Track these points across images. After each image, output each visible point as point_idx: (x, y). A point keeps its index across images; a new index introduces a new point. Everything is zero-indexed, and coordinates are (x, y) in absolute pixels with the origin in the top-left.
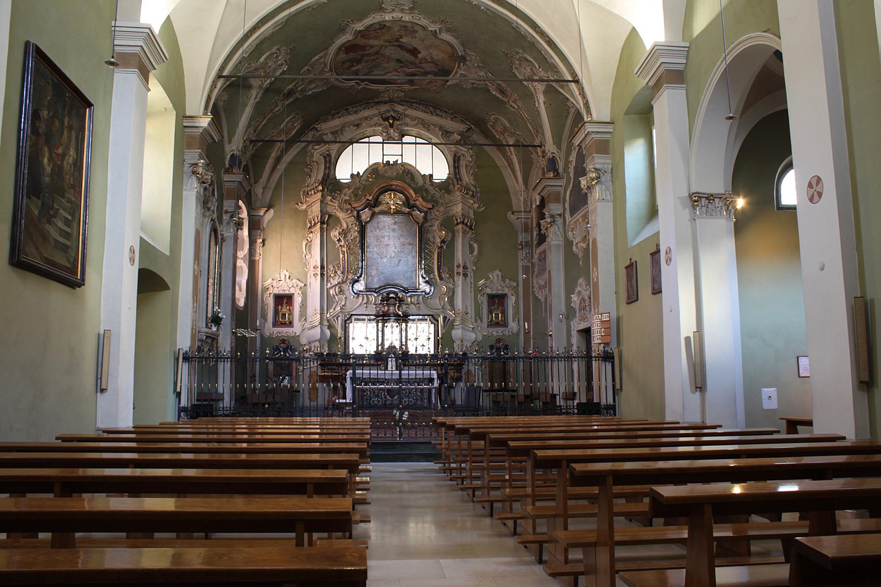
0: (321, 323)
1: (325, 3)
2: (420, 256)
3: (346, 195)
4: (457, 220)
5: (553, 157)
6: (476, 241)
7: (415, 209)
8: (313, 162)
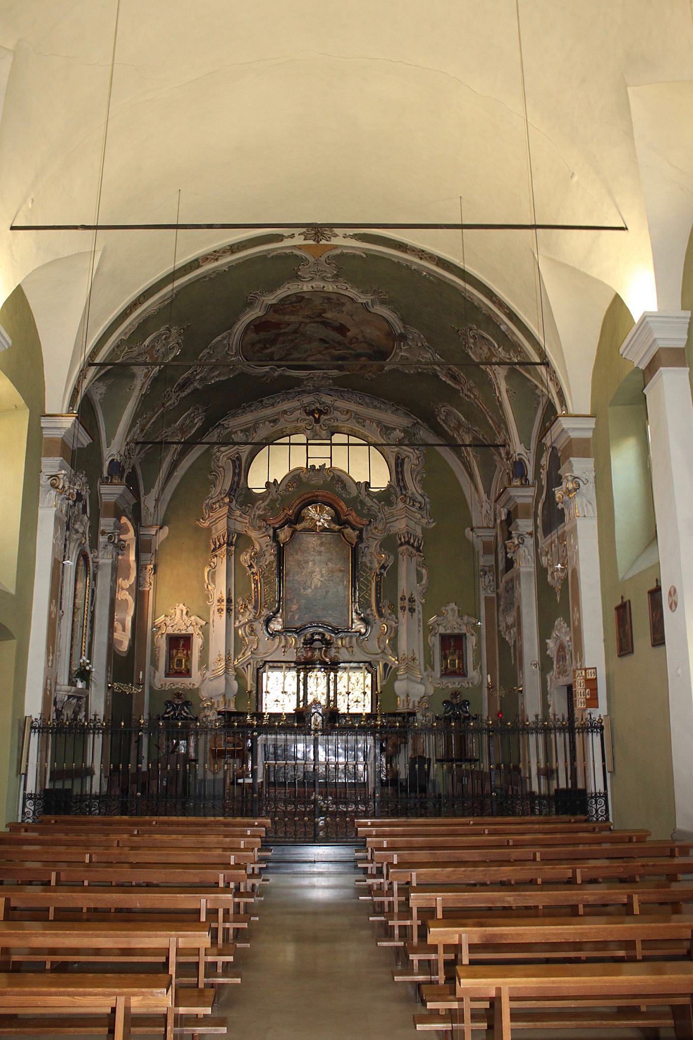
0: (226, 671)
1: (225, 271)
2: (354, 586)
3: (260, 509)
4: (400, 539)
5: (520, 459)
6: (424, 565)
7: (347, 526)
8: (219, 467)
